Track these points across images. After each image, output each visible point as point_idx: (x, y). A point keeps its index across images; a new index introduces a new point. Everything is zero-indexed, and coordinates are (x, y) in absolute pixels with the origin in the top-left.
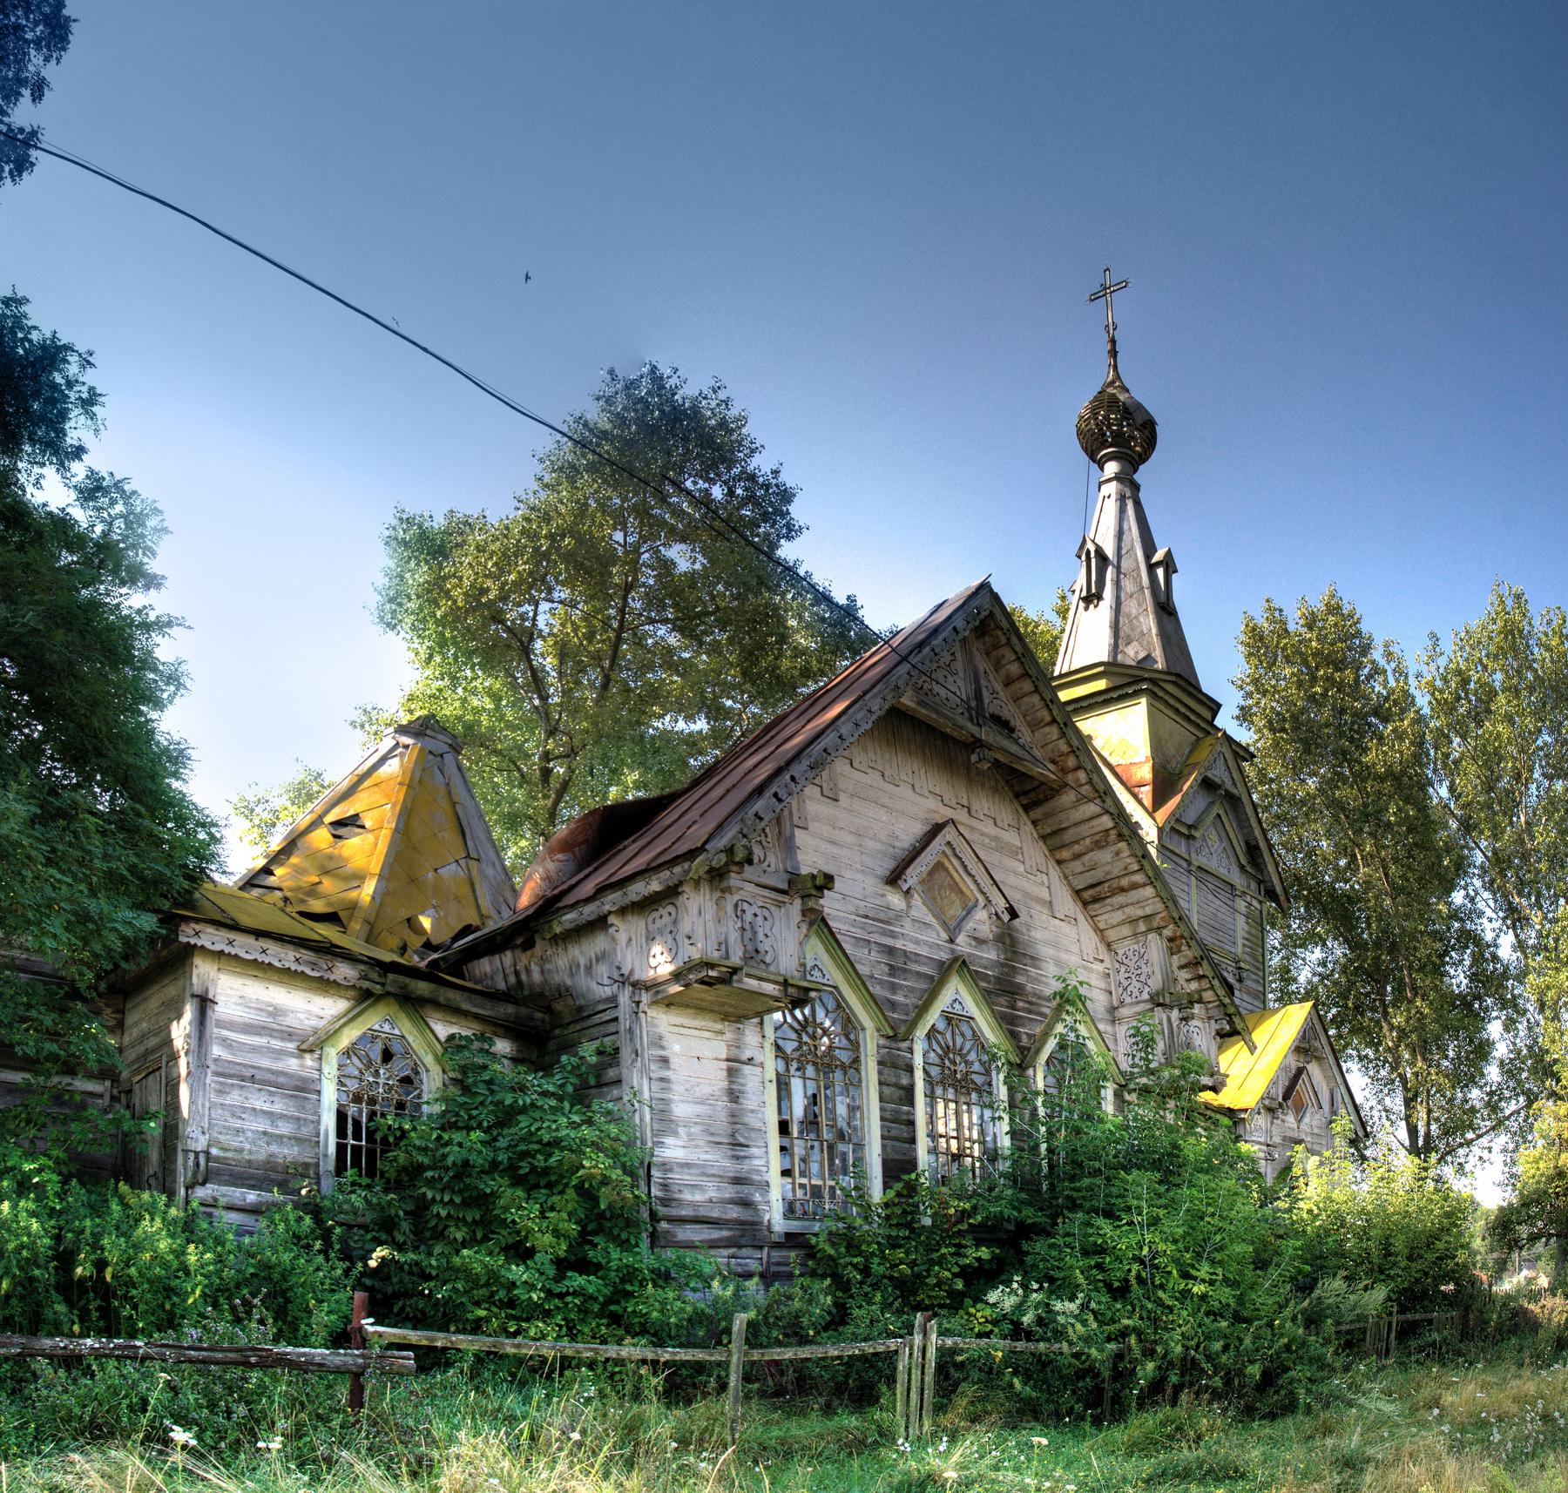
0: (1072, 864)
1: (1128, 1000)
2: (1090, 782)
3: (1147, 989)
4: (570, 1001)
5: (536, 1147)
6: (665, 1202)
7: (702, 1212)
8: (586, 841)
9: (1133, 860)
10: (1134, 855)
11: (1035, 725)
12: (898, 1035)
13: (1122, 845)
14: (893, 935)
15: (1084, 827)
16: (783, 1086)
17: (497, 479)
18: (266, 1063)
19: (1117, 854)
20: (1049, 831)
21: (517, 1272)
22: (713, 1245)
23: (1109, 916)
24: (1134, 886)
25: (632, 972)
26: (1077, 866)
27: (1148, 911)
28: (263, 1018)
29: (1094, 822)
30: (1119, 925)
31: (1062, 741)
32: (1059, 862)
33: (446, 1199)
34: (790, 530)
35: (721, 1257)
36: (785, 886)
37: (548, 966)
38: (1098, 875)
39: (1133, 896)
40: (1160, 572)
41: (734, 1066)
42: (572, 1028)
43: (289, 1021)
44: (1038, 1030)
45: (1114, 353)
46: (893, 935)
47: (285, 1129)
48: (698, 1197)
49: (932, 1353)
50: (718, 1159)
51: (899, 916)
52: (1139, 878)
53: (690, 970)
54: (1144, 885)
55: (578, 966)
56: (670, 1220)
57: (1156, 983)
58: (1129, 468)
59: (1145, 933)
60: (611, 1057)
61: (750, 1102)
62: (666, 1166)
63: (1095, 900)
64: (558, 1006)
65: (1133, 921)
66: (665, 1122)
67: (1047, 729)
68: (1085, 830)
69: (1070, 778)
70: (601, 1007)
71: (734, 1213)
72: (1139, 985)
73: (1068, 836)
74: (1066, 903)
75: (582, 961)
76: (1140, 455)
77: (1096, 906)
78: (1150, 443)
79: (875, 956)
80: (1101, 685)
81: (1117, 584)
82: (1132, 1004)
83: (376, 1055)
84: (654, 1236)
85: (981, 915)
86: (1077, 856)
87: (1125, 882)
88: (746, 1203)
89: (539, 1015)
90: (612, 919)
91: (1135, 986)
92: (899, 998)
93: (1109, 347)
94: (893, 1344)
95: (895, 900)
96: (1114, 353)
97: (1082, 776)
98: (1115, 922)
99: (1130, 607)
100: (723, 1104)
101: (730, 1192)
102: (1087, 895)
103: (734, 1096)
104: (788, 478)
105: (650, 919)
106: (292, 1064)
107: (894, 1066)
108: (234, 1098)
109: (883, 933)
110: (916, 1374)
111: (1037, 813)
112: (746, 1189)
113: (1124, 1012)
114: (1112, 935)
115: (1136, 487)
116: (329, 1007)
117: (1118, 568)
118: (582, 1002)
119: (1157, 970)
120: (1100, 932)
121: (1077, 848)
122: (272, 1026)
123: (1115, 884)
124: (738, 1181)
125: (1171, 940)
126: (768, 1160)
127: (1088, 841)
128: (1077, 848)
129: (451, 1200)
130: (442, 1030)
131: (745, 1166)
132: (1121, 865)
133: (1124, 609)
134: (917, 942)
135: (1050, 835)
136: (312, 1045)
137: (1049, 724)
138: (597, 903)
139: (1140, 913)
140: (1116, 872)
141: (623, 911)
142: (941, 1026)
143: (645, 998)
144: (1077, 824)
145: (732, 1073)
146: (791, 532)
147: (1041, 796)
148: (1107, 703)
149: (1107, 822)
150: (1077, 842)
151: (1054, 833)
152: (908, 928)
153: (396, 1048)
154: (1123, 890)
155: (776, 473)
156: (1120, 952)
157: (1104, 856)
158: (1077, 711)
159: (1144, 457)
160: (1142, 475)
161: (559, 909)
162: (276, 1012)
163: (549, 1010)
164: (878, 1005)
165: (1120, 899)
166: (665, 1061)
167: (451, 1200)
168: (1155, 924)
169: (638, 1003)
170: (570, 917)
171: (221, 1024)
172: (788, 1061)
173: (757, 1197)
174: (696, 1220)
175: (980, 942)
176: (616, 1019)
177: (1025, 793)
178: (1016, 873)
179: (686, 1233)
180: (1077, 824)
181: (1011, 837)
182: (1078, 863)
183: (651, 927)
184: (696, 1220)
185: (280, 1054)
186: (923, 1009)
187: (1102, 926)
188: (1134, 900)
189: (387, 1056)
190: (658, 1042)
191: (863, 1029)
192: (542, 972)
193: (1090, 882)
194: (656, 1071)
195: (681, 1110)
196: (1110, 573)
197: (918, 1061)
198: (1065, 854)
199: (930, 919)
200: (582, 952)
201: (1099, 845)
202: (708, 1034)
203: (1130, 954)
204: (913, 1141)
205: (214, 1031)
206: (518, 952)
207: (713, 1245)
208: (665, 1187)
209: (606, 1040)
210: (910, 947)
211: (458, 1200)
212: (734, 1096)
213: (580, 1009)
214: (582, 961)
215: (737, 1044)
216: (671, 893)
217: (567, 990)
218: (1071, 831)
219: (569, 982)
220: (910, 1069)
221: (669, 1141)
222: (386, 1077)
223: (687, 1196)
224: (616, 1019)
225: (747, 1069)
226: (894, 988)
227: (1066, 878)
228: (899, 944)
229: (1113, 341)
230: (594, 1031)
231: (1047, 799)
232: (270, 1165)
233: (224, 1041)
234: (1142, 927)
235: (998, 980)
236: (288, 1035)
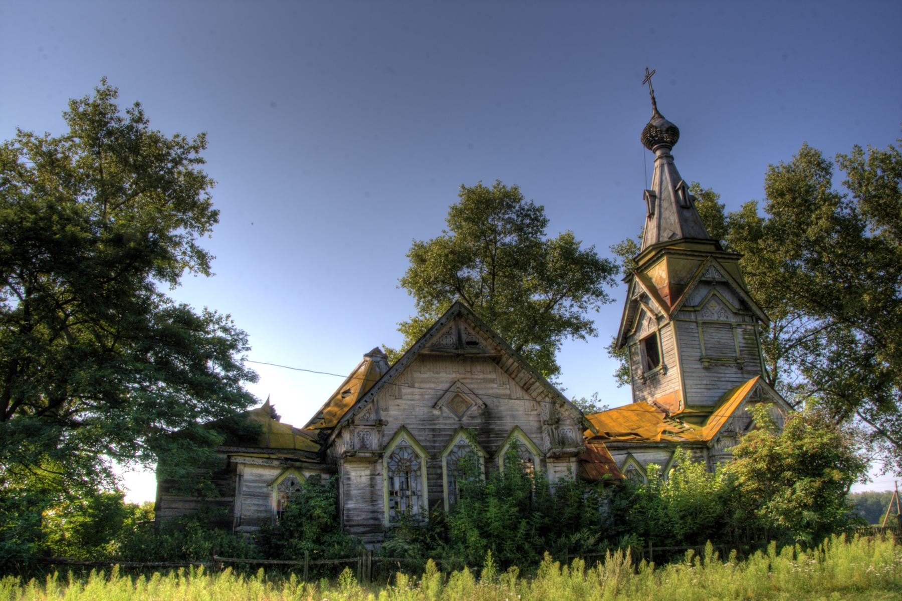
6: (348, 521)
7: (361, 523)
12: (434, 457)
14: (435, 424)
16: (391, 479)
17: (436, 227)
18: (257, 490)
22: (364, 533)
28: (257, 478)
35: (369, 537)
40: (680, 192)
41: (373, 477)
43: (264, 478)
44: (500, 443)
45: (654, 103)
46: (435, 424)
47: (262, 508)
48: (359, 518)
49: (369, 562)
50: (367, 507)
51: (438, 417)
56: (350, 526)
62: (348, 510)
66: (348, 496)
71: (372, 522)
74: (519, 392)
79: (427, 433)
80: (653, 253)
81: (660, 206)
83: (289, 484)
84: (344, 531)
85: (475, 408)
88: (375, 519)
92: (437, 444)
93: (651, 101)
94: (355, 559)
95: (436, 412)
96: (654, 103)
99: (666, 214)
100: (369, 489)
101: (371, 515)
103: (372, 486)
106: (265, 490)
107: (434, 468)
108: (248, 501)
109: (431, 424)
110: (364, 568)
112: (375, 515)
116: (275, 472)
117: (660, 199)
122: (259, 479)
124: (373, 512)
126: (385, 504)
130: (307, 474)
131: (376, 507)
133: (663, 216)
134: (445, 424)
136: (270, 483)
142: (456, 450)
145: (372, 479)
148: (654, 262)
152: (441, 421)
153: (295, 482)
158: (646, 268)
159: (673, 142)
162: (261, 476)
164: (424, 448)
166: (349, 479)
171: (246, 481)
172: (393, 472)
173: (380, 516)
174: (358, 525)
175: (473, 418)
178: (492, 388)
179: (353, 530)
181: (493, 376)
184: (358, 525)
185: (261, 487)
186: (445, 447)
189: (293, 484)
190: (347, 473)
194: (346, 482)
195: (354, 492)
196: (657, 203)
197: (444, 464)
199: (452, 415)
201: (519, 372)
204: (442, 492)
205: (242, 482)
207: (364, 533)
208: (348, 516)
210: (442, 427)
212: (372, 486)
215: (374, 469)
220: (441, 467)
221: (350, 502)
222: (292, 490)
223: (355, 518)
225: (377, 477)
226: (434, 442)
228: (437, 427)
229: (653, 98)
232: (258, 519)
233: (247, 486)
235: (481, 429)
236: (264, 482)
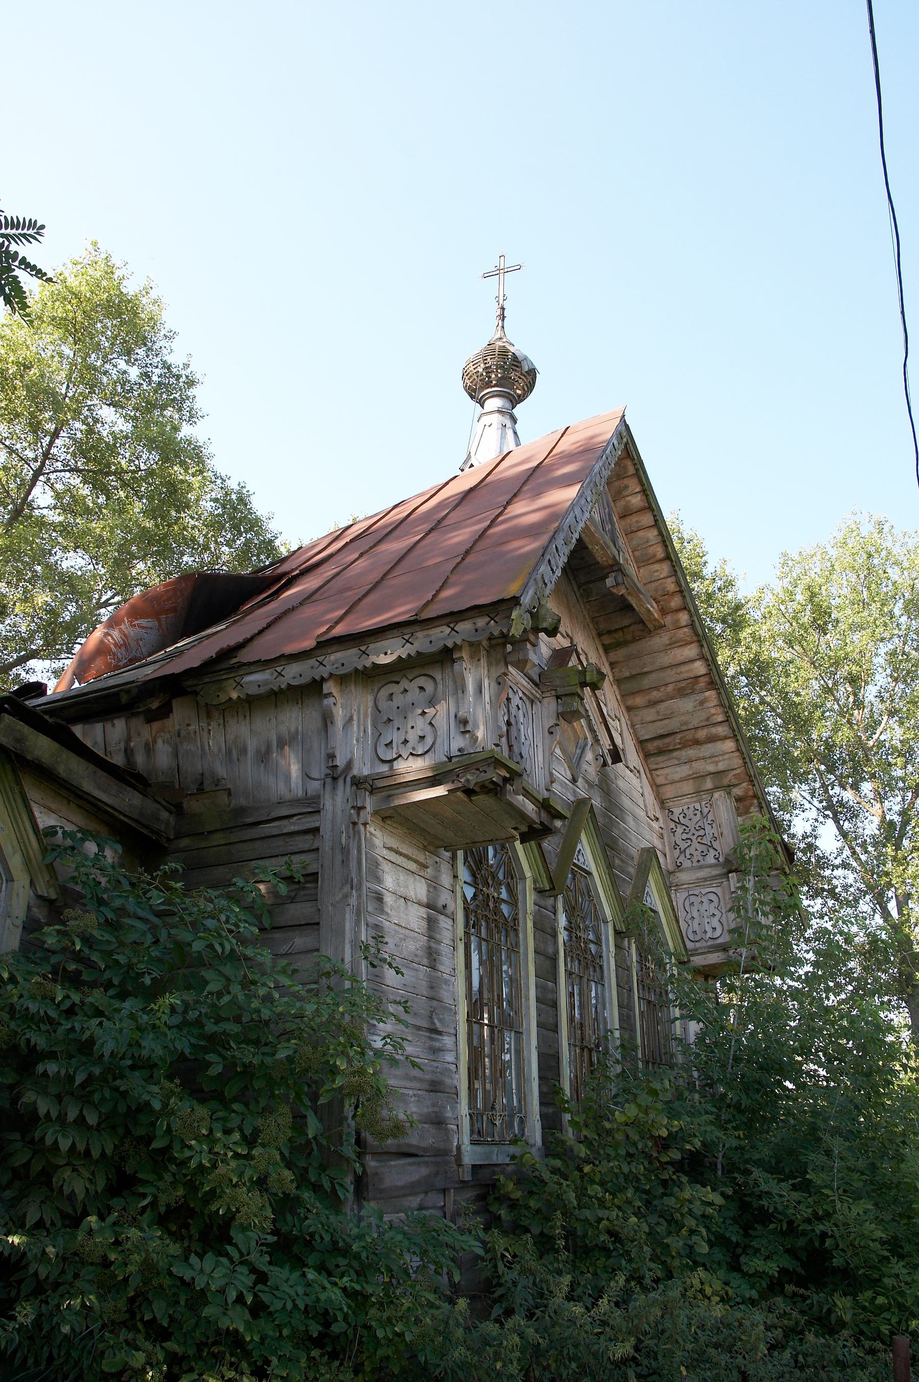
0: (646, 711)
1: (687, 864)
2: (692, 625)
3: (712, 853)
4: (224, 798)
5: (233, 1028)
8: (174, 610)
9: (719, 710)
10: (721, 705)
11: (644, 561)
13: (711, 694)
15: (669, 672)
19: (702, 703)
20: (628, 674)
21: (208, 1272)
23: (674, 770)
24: (713, 739)
25: (349, 765)
26: (649, 714)
27: (721, 766)
29: (684, 668)
30: (682, 780)
31: (673, 579)
32: (629, 709)
33: (72, 1115)
34: (191, 417)
36: (536, 678)
37: (186, 747)
38: (672, 725)
39: (707, 750)
42: (218, 839)
45: (503, 317)
52: (721, 730)
53: (467, 768)
54: (726, 738)
55: (244, 750)
57: (725, 845)
58: (508, 405)
59: (711, 791)
60: (305, 884)
61: (445, 966)
63: (660, 752)
64: (193, 806)
65: (699, 777)
67: (657, 567)
68: (670, 676)
69: (668, 620)
70: (284, 812)
72: (701, 848)
73: (646, 682)
75: (252, 745)
76: (519, 396)
77: (660, 759)
78: (530, 387)
82: (692, 868)
86: (653, 704)
87: (702, 734)
89: (165, 815)
90: (329, 687)
91: (696, 848)
97: (684, 617)
98: (677, 777)
102: (651, 747)
104: (196, 369)
105: (384, 693)
111: (619, 654)
113: (683, 877)
114: (669, 792)
115: (514, 420)
118: (243, 802)
119: (726, 831)
120: (656, 787)
121: (655, 695)
123: (689, 736)
125: (739, 799)
127: (670, 688)
128: (655, 695)
129: (81, 1121)
132: (703, 715)
135: (627, 678)
137: (661, 561)
138: (312, 662)
139: (711, 768)
140: (695, 722)
141: (343, 680)
143: (370, 803)
144: (663, 669)
146: (192, 417)
147: (629, 637)
149: (699, 668)
150: (657, 688)
151: (633, 677)
154: (697, 742)
155: (186, 366)
156: (677, 811)
157: (687, 704)
159: (520, 399)
160: (519, 411)
161: (242, 665)
163: (178, 810)
165: (691, 752)
167: (81, 1121)
168: (726, 782)
169: (359, 809)
170: (256, 680)
176: (316, 831)
177: (609, 632)
180: (663, 669)
182: (652, 711)
183: (383, 704)
187: (660, 781)
188: (707, 754)
191: (524, 878)
192: (176, 754)
193: (661, 732)
198: (639, 700)
200: (252, 732)
201: (682, 693)
202: (413, 866)
203: (690, 813)
206: (138, 723)
209: (295, 858)
211: (92, 1119)
213: (241, 811)
214: (252, 745)
216: (445, 657)
217: (217, 782)
218: (653, 676)
219: (221, 771)
224: (316, 831)
227: (633, 726)
229: (503, 309)
230: (278, 845)
231: (634, 640)
234: (709, 784)
